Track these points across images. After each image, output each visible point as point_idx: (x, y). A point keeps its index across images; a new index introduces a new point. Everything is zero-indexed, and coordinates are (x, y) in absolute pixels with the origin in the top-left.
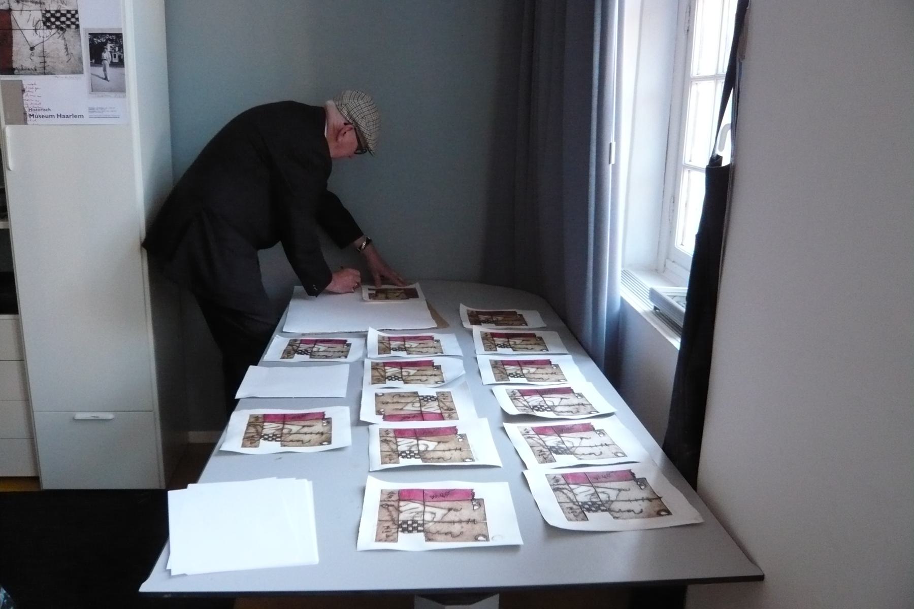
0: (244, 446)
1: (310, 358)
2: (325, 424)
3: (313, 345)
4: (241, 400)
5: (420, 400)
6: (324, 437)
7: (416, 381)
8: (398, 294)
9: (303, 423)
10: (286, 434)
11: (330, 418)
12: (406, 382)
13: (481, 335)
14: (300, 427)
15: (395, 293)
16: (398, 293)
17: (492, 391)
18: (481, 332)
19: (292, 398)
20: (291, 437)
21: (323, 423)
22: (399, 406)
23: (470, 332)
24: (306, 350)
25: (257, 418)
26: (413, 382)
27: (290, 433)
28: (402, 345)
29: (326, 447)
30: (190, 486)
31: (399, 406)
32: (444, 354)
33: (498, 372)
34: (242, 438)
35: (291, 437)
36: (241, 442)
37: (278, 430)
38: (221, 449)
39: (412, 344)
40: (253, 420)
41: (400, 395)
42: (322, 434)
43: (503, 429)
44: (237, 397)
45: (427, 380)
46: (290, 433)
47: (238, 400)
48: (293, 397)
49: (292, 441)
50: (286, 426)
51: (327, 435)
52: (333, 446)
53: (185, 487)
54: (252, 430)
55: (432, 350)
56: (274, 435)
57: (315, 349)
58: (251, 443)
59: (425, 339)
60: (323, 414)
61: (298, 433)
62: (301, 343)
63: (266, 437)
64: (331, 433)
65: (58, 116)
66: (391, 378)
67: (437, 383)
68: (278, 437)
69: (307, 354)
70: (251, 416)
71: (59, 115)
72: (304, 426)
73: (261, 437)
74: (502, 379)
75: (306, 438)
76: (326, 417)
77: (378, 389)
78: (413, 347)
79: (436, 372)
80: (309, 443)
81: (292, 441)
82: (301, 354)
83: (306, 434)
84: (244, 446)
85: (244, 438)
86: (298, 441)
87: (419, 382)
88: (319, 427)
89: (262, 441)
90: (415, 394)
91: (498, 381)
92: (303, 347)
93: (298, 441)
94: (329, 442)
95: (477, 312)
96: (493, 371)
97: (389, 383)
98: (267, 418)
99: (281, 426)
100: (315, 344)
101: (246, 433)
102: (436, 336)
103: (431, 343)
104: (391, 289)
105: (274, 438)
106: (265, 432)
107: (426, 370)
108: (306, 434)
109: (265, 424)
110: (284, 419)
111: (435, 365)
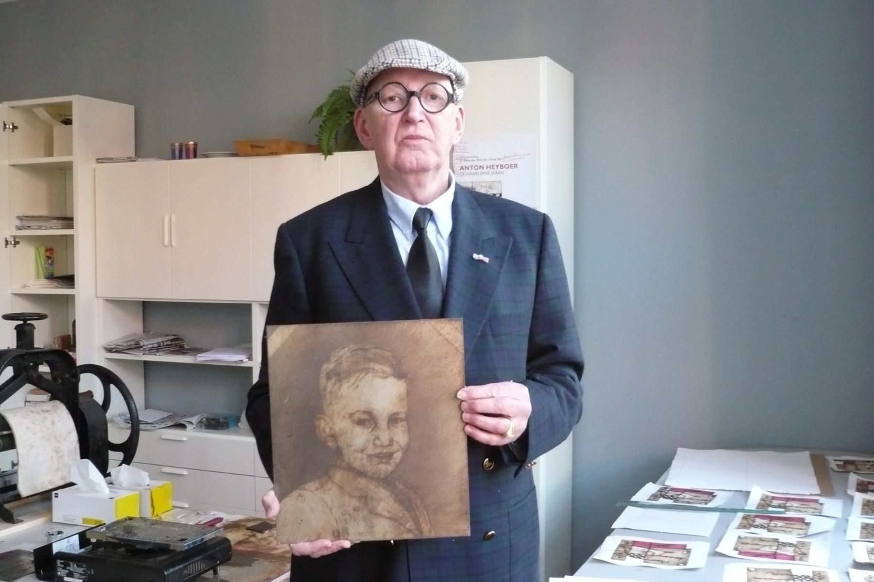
0: (613, 558)
1: (674, 502)
2: (685, 553)
3: (680, 493)
4: (616, 530)
5: (779, 545)
6: (682, 561)
7: (780, 532)
8: (868, 467)
9: (665, 550)
10: (649, 555)
11: (690, 549)
12: (769, 531)
13: (863, 501)
14: (662, 552)
15: (865, 465)
16: (869, 465)
17: (851, 546)
18: (864, 499)
19: (660, 532)
20: (653, 558)
21: (683, 552)
22: (757, 547)
23: (852, 498)
24: (672, 496)
25: (627, 542)
26: (775, 531)
27: (653, 555)
28: (783, 504)
29: (682, 567)
30: (566, 576)
31: (757, 547)
32: (822, 514)
33: (866, 532)
34: (612, 553)
35: (653, 558)
36: (611, 556)
37: (643, 552)
38: (33, 109)
39: (793, 503)
40: (623, 543)
41: (761, 540)
42: (680, 558)
43: (848, 574)
44: (613, 527)
45: (790, 532)
46: (653, 555)
47: (614, 529)
48: (662, 531)
49: (653, 560)
50: (651, 550)
51: (685, 560)
52: (688, 566)
53: (563, 577)
54: (622, 549)
55: (812, 510)
56: (639, 555)
57: (680, 496)
58: (619, 557)
59: (809, 502)
60: (685, 546)
61: (660, 556)
62: (670, 490)
63: (633, 555)
64: (688, 559)
65: (487, 167)
66: (757, 527)
67: (799, 534)
68: (643, 557)
69: (671, 499)
70: (623, 541)
71: (489, 166)
72: (666, 552)
73: (628, 554)
74: (867, 537)
75: (667, 559)
76: (687, 548)
77: (743, 533)
78: (794, 506)
79: (804, 527)
80: (668, 563)
81: (653, 560)
82: (666, 498)
83: (666, 557)
84: (613, 558)
85: (614, 554)
86: (658, 561)
87: (783, 532)
88: (679, 554)
89: (628, 557)
90: (776, 540)
91: (862, 538)
92: (670, 493)
93: (658, 561)
94: (685, 564)
95: (868, 482)
96: (861, 531)
97: (753, 530)
98: (635, 543)
99: (647, 550)
100: (683, 493)
101: (616, 550)
102: (822, 500)
103: (813, 505)
104: (860, 461)
105: (639, 556)
106: (632, 552)
107: (795, 524)
108: (666, 557)
109: (633, 547)
110: (650, 546)
111: (806, 521)
